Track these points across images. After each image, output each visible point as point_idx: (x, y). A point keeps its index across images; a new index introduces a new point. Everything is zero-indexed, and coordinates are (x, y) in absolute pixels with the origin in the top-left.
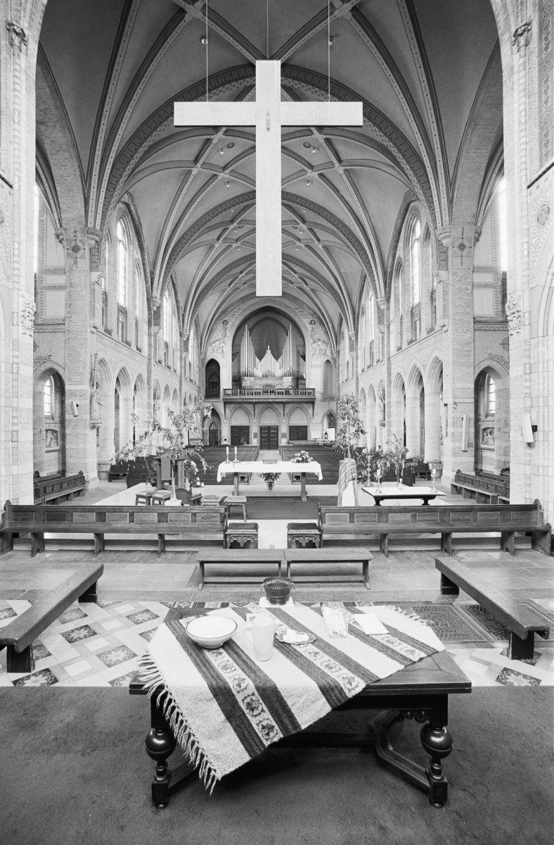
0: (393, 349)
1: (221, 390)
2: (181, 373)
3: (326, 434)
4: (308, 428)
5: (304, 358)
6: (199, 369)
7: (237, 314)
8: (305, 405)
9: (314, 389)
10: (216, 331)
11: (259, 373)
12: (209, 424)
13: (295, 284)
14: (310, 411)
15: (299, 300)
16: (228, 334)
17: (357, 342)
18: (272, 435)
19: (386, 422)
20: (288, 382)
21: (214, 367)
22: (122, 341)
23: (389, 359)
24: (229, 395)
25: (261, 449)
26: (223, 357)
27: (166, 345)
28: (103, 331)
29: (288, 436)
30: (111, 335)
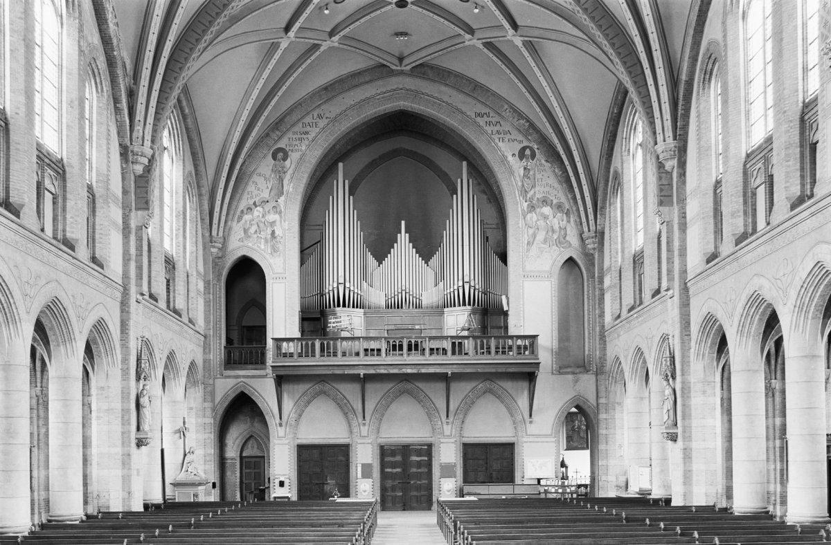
0: (695, 260)
1: (270, 343)
2: (126, 276)
3: (563, 465)
4: (352, 450)
5: (504, 258)
6: (207, 283)
7: (313, 132)
8: (508, 385)
9: (535, 337)
10: (255, 178)
11: (377, 297)
12: (239, 442)
13: (478, 34)
14: (523, 401)
15: (488, 90)
16: (288, 187)
17: (683, 174)
18: (414, 470)
19: (679, 430)
20: (457, 320)
21: (250, 283)
22: (55, 238)
23: (685, 289)
24: (291, 355)
25: (384, 508)
26: (275, 250)
27: (170, 264)
28: (187, 322)
29: (459, 471)
30: (18, 216)
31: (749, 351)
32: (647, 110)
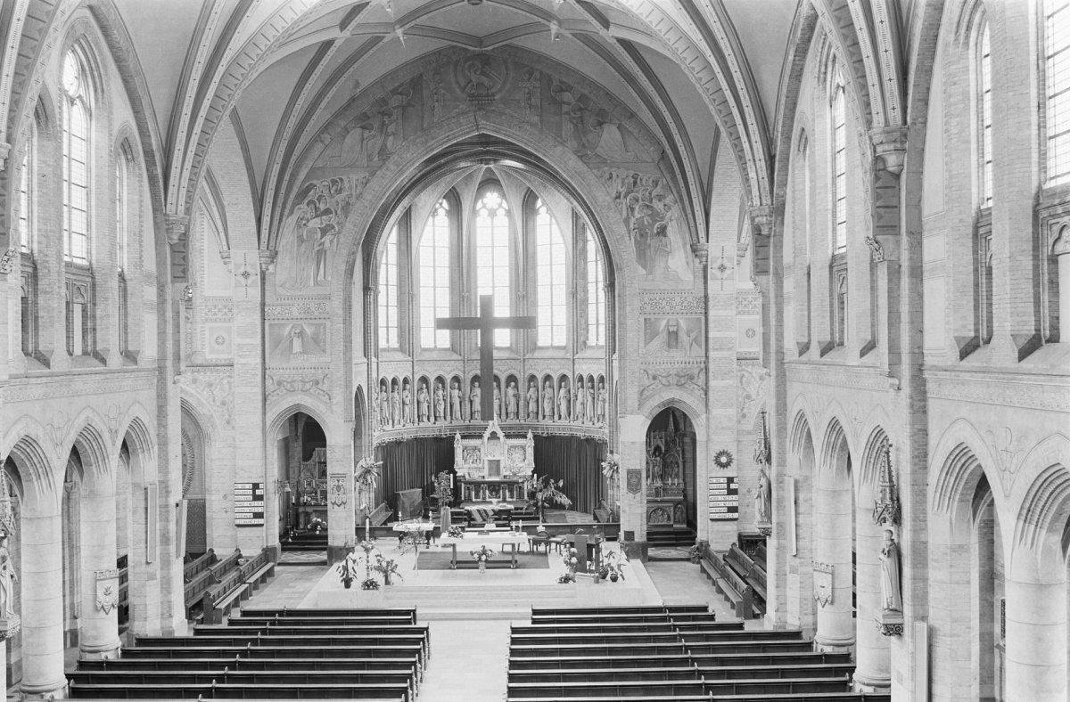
31: (1040, 553)
32: (843, 31)
